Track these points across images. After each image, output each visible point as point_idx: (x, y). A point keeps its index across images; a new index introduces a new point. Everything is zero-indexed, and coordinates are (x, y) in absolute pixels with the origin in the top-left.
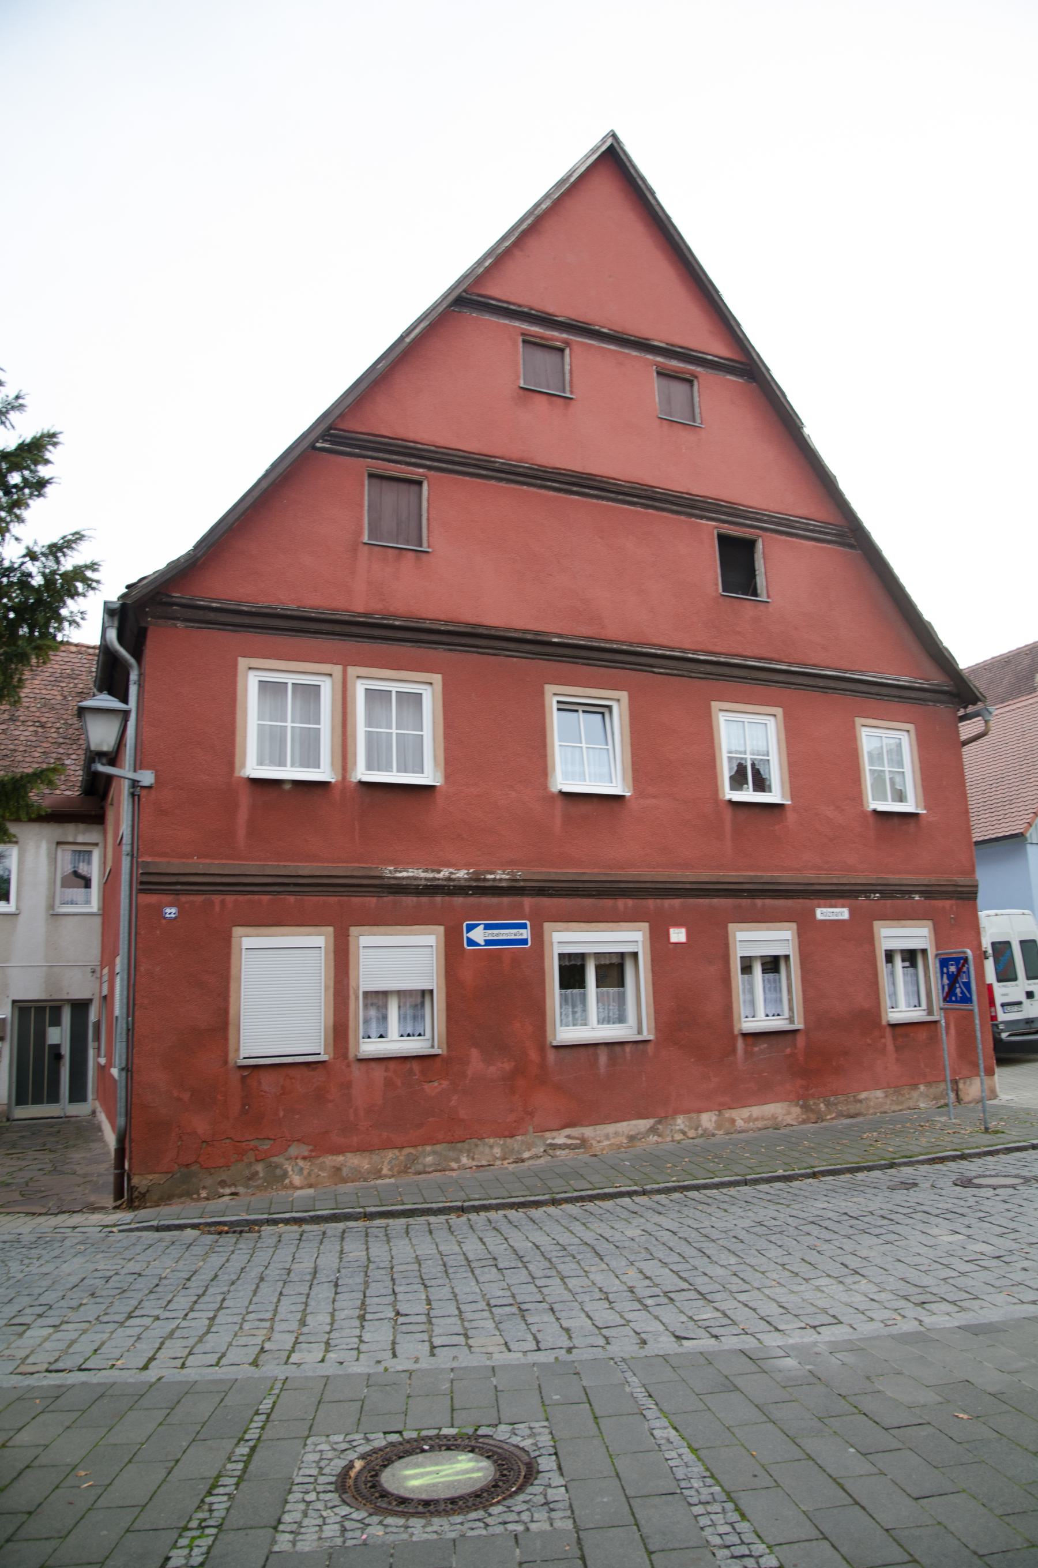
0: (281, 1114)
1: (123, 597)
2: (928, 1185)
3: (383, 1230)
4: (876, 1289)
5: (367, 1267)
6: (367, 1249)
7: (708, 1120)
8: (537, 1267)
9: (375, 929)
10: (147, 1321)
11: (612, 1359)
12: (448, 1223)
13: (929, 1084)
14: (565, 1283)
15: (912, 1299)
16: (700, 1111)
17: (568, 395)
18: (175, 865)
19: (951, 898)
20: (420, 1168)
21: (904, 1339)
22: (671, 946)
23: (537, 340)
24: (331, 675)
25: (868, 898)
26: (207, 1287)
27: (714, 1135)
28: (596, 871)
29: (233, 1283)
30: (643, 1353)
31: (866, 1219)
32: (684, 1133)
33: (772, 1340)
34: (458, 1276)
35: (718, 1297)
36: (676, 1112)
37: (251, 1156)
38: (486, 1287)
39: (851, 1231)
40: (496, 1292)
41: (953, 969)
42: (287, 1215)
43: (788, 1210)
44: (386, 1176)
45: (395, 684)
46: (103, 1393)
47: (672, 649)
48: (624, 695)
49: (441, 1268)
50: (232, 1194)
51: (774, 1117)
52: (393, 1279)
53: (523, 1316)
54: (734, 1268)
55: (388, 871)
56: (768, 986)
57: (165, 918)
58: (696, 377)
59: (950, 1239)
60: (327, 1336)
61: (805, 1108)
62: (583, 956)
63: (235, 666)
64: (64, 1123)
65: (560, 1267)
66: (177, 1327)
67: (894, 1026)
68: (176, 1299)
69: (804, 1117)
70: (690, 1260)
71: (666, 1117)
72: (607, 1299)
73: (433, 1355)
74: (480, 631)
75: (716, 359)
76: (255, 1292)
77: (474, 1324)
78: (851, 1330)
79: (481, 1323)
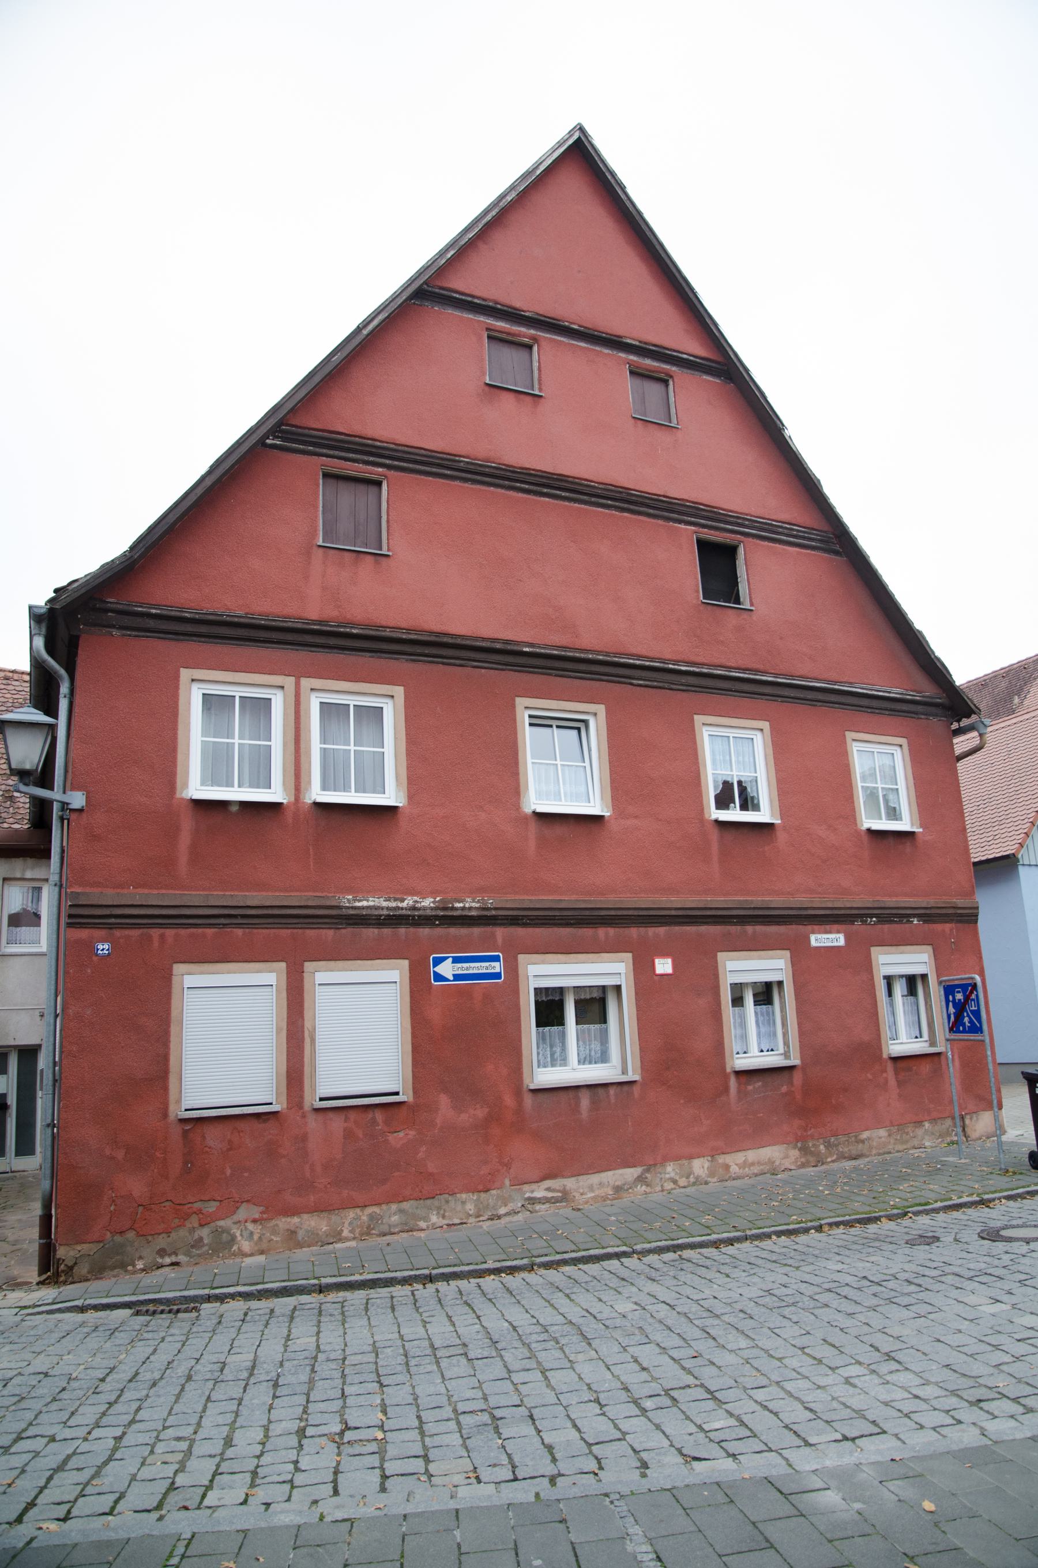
0: (228, 1172)
1: (51, 601)
2: (950, 1239)
3: (339, 1306)
4: (920, 1381)
5: (315, 1358)
6: (318, 1333)
7: (700, 1166)
8: (514, 1356)
9: (332, 963)
10: (38, 1444)
11: (606, 1495)
12: (413, 1294)
13: (934, 1121)
14: (546, 1378)
15: (965, 1394)
16: (691, 1157)
17: (537, 392)
18: (109, 896)
19: (951, 921)
20: (385, 1228)
21: (967, 1456)
23: (504, 336)
24: (283, 687)
25: (864, 922)
26: (122, 1391)
27: (706, 1183)
28: (574, 897)
29: (154, 1384)
30: (645, 1484)
32: (675, 1182)
33: (805, 1461)
34: (422, 1369)
36: (665, 1159)
37: (194, 1221)
38: (451, 1385)
39: (875, 1301)
40: (463, 1390)
41: (959, 996)
42: (231, 1290)
43: (798, 1273)
44: (347, 1239)
45: (353, 696)
47: (652, 659)
48: (601, 709)
49: (401, 1359)
50: (173, 1264)
51: (771, 1162)
52: (344, 1376)
53: (497, 1428)
54: (746, 1354)
55: (347, 900)
56: (761, 1018)
57: (97, 955)
60: (256, 1461)
61: (804, 1150)
62: (561, 990)
63: (177, 677)
64: (8, 1179)
65: (542, 1356)
66: (74, 1453)
67: (895, 1059)
68: (81, 1410)
69: (803, 1160)
70: (692, 1343)
71: (655, 1165)
73: (383, 1489)
74: (445, 640)
76: (178, 1397)
77: (437, 1440)
78: (899, 1443)
79: (446, 1439)
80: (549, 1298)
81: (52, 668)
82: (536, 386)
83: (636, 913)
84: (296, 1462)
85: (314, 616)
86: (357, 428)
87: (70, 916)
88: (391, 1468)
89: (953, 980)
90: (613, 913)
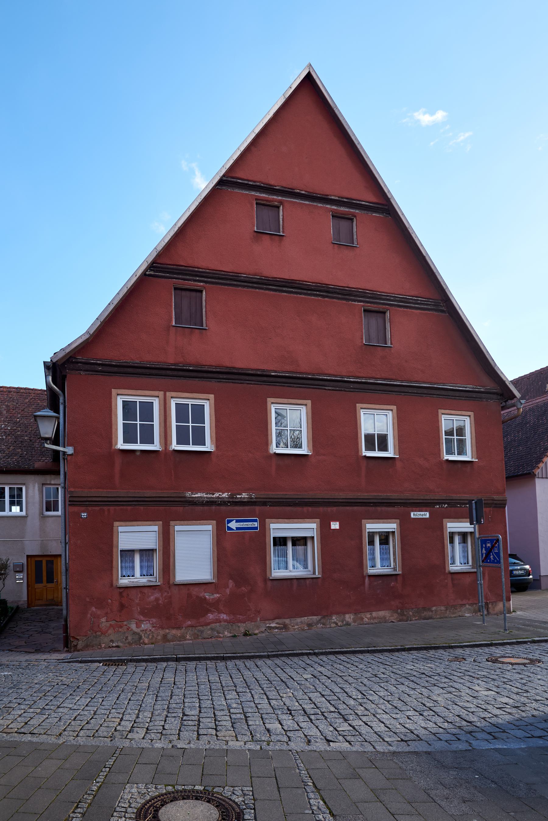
7: (349, 618)
9: (182, 522)
10: (66, 710)
11: (290, 751)
16: (344, 613)
17: (281, 234)
22: (331, 531)
30: (308, 748)
31: (436, 678)
35: (351, 718)
36: (331, 614)
41: (489, 545)
46: (36, 748)
55: (188, 494)
57: (82, 518)
58: (355, 216)
59: (486, 693)
60: (147, 724)
61: (402, 614)
65: (268, 693)
66: (78, 715)
72: (290, 714)
73: (198, 739)
75: (367, 204)
77: (221, 723)
79: (224, 723)
80: (274, 670)
81: (57, 392)
82: (281, 230)
83: (322, 500)
84: (163, 726)
85: (172, 361)
86: (190, 262)
87: (70, 501)
88: (201, 732)
89: (488, 537)
90: (311, 500)
